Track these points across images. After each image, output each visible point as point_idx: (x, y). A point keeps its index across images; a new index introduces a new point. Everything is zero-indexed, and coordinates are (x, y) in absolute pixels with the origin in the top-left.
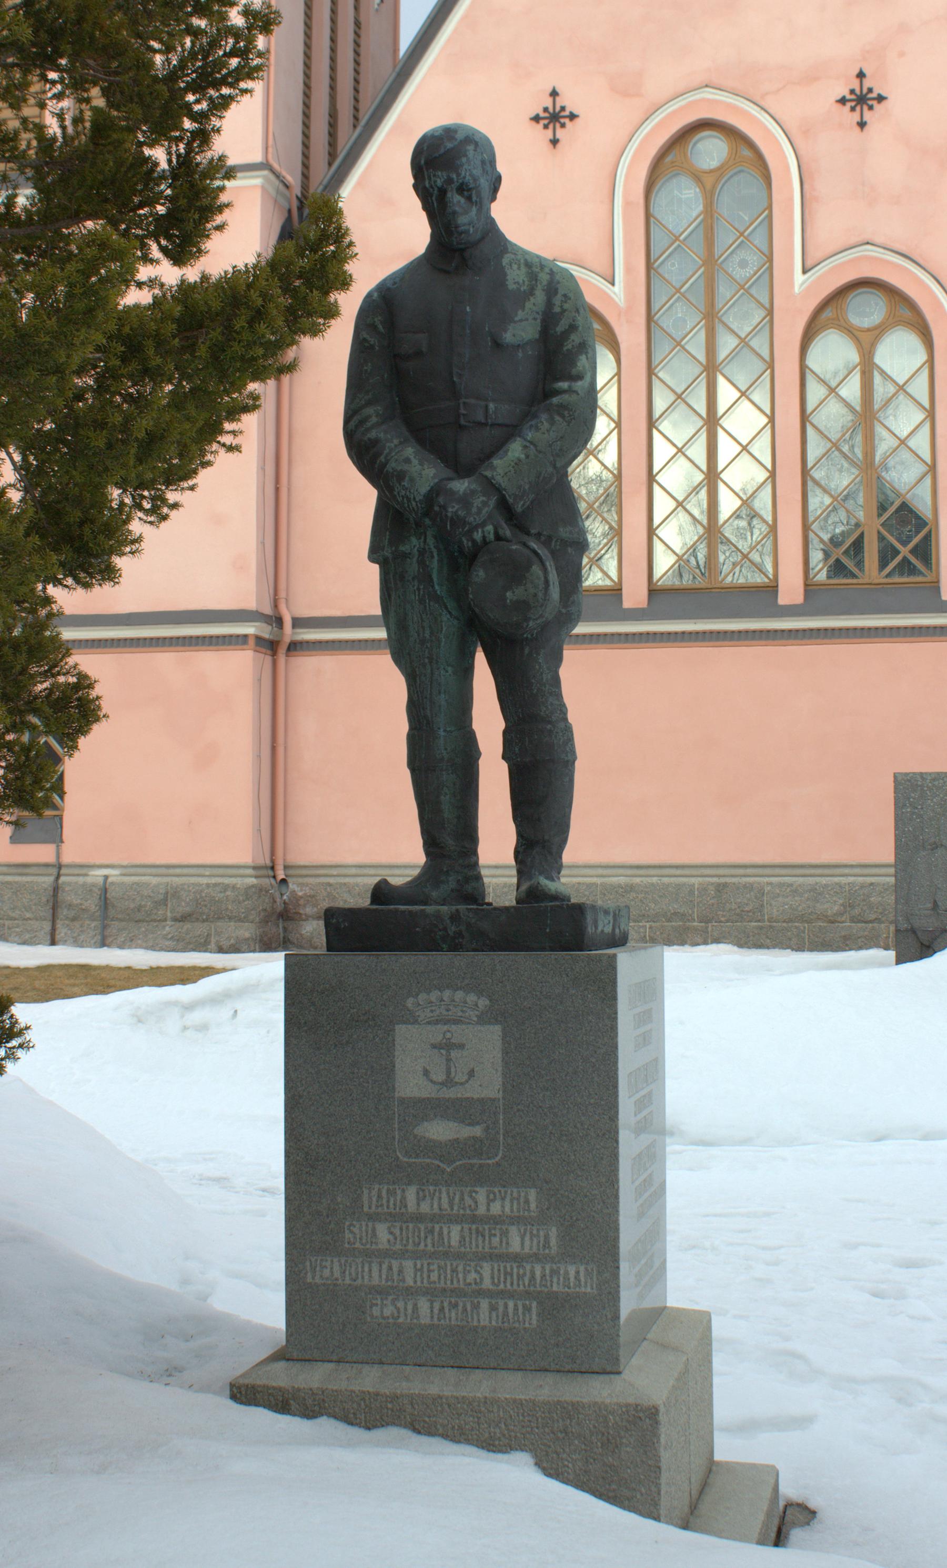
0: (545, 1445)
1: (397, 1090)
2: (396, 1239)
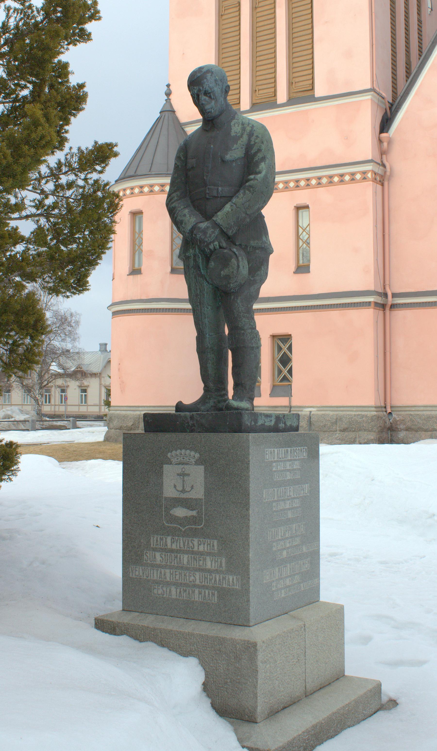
0: (212, 656)
1: (164, 494)
2: (163, 559)
